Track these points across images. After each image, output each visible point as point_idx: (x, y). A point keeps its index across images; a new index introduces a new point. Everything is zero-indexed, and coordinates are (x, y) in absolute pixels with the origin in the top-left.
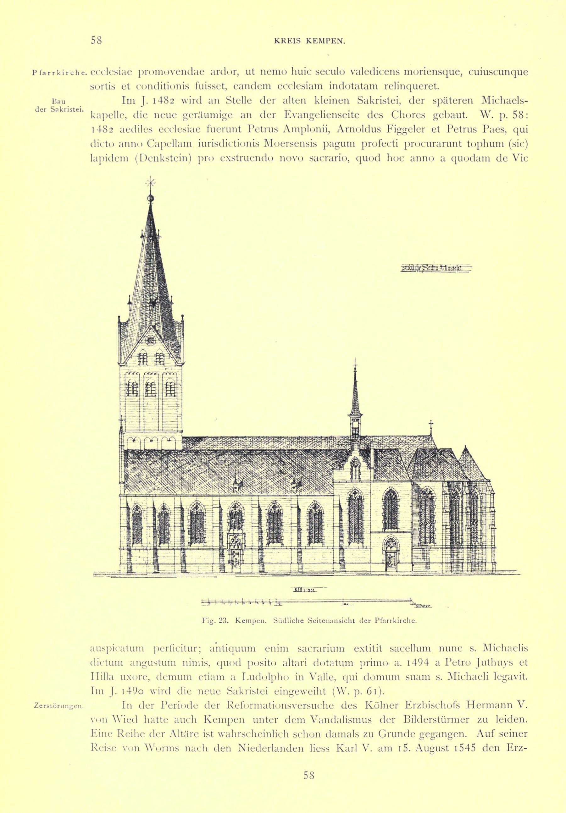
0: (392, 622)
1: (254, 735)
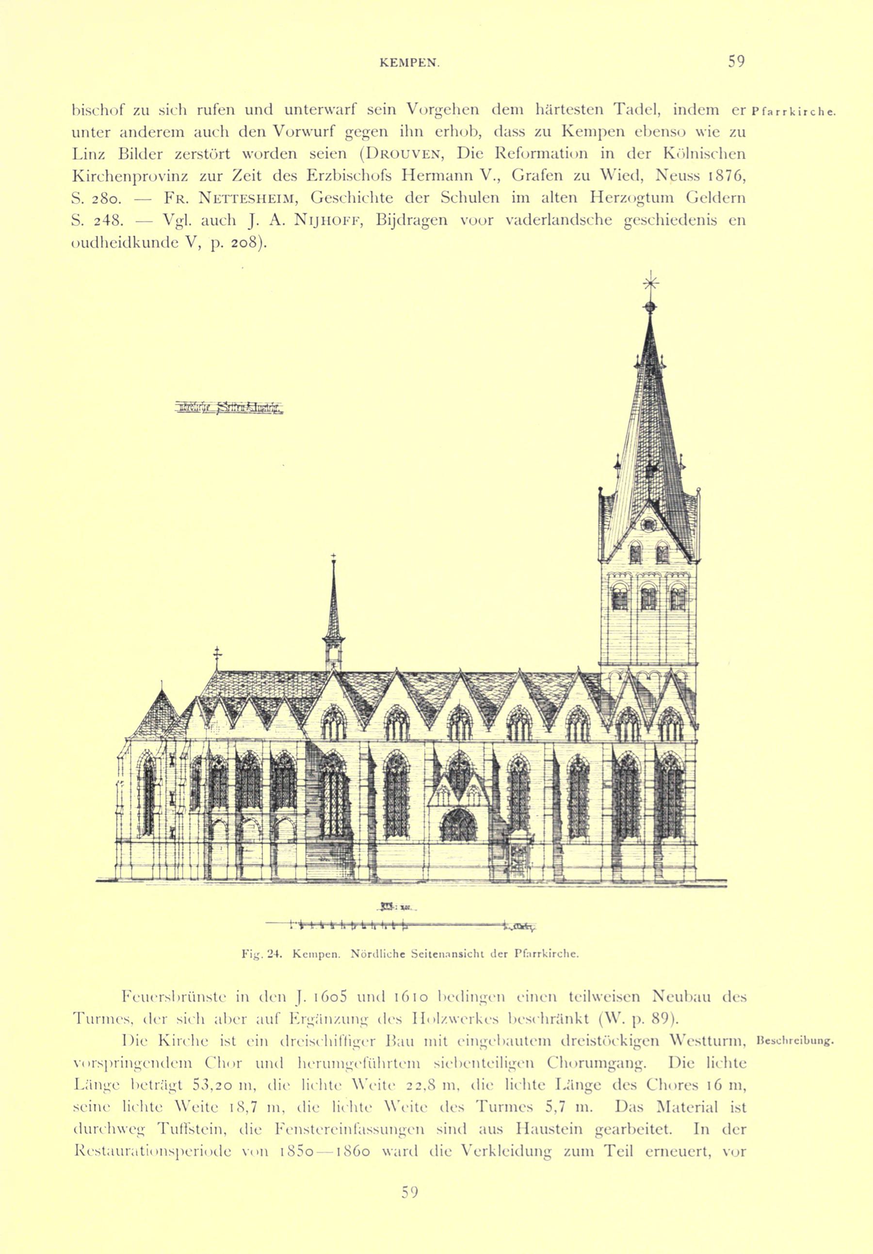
0: (541, 955)
1: (723, 155)
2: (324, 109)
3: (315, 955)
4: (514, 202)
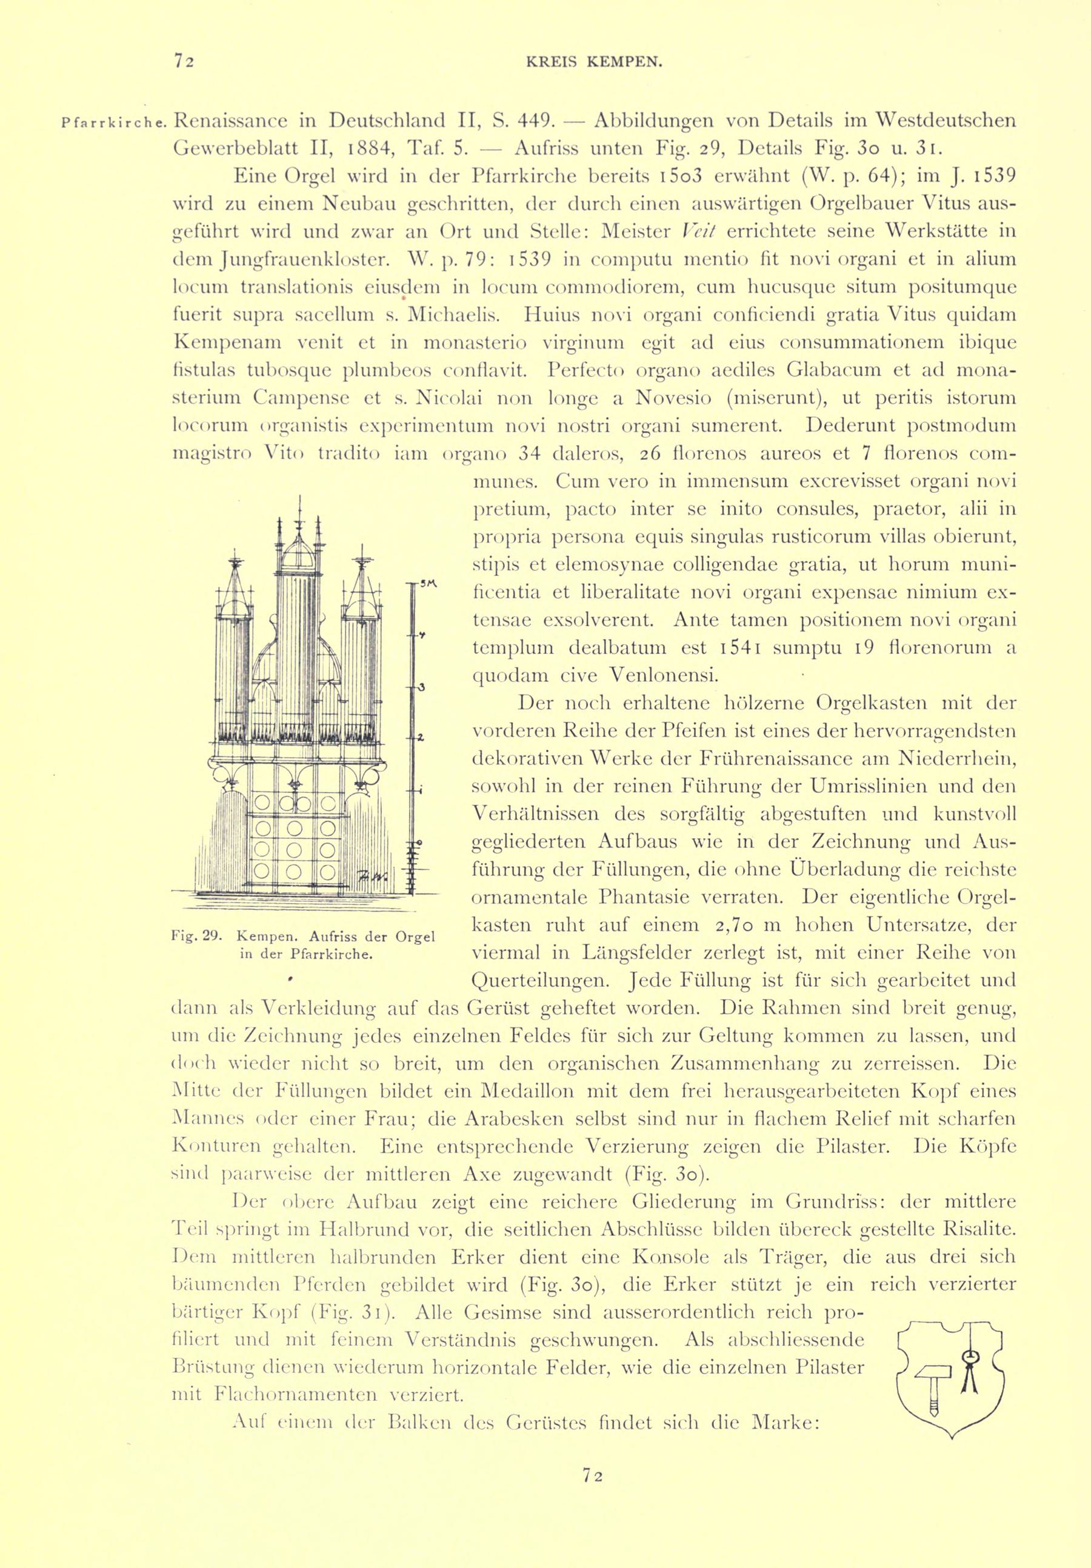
2: (733, 175)
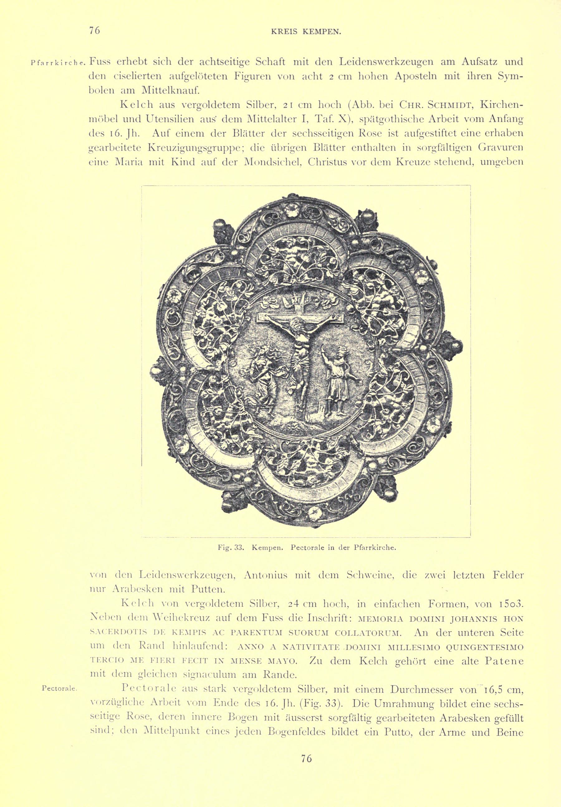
0: (371, 549)
3: (266, 548)
4: (469, 79)
